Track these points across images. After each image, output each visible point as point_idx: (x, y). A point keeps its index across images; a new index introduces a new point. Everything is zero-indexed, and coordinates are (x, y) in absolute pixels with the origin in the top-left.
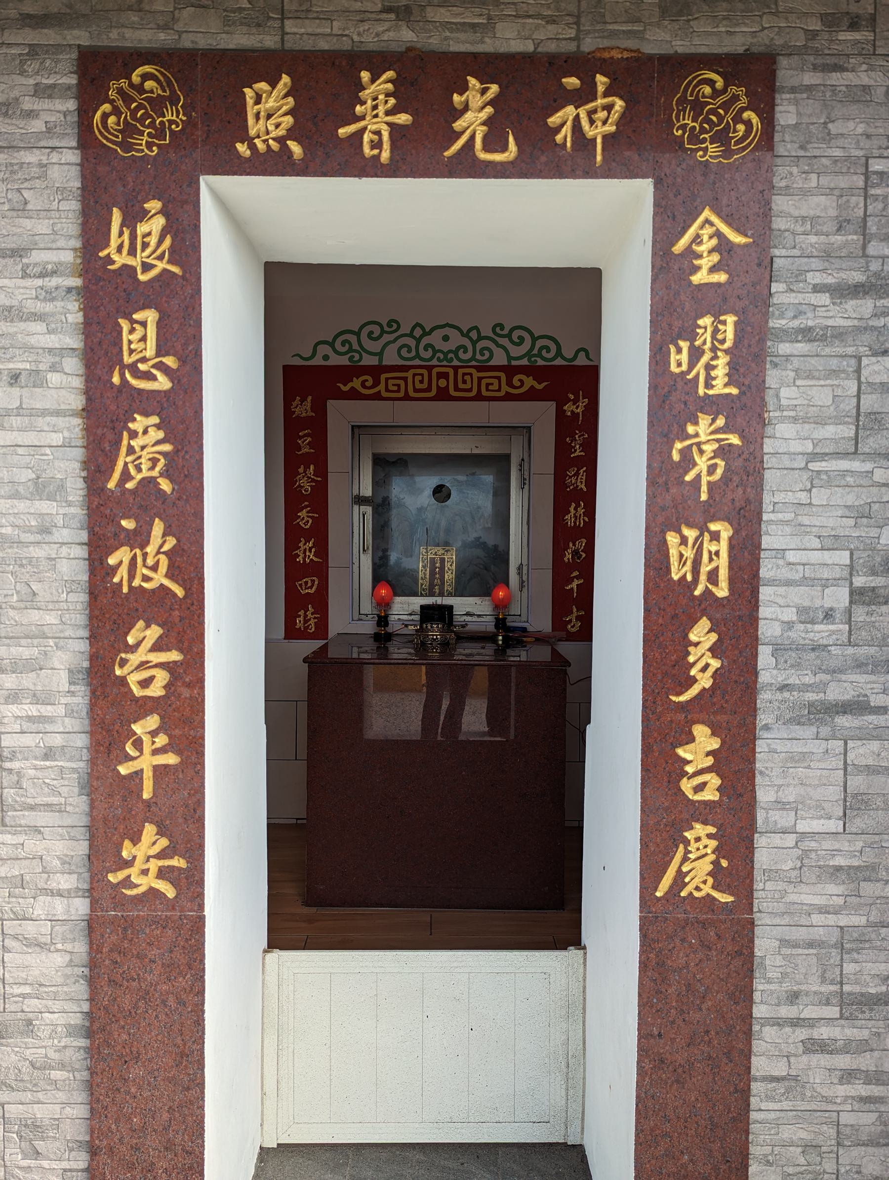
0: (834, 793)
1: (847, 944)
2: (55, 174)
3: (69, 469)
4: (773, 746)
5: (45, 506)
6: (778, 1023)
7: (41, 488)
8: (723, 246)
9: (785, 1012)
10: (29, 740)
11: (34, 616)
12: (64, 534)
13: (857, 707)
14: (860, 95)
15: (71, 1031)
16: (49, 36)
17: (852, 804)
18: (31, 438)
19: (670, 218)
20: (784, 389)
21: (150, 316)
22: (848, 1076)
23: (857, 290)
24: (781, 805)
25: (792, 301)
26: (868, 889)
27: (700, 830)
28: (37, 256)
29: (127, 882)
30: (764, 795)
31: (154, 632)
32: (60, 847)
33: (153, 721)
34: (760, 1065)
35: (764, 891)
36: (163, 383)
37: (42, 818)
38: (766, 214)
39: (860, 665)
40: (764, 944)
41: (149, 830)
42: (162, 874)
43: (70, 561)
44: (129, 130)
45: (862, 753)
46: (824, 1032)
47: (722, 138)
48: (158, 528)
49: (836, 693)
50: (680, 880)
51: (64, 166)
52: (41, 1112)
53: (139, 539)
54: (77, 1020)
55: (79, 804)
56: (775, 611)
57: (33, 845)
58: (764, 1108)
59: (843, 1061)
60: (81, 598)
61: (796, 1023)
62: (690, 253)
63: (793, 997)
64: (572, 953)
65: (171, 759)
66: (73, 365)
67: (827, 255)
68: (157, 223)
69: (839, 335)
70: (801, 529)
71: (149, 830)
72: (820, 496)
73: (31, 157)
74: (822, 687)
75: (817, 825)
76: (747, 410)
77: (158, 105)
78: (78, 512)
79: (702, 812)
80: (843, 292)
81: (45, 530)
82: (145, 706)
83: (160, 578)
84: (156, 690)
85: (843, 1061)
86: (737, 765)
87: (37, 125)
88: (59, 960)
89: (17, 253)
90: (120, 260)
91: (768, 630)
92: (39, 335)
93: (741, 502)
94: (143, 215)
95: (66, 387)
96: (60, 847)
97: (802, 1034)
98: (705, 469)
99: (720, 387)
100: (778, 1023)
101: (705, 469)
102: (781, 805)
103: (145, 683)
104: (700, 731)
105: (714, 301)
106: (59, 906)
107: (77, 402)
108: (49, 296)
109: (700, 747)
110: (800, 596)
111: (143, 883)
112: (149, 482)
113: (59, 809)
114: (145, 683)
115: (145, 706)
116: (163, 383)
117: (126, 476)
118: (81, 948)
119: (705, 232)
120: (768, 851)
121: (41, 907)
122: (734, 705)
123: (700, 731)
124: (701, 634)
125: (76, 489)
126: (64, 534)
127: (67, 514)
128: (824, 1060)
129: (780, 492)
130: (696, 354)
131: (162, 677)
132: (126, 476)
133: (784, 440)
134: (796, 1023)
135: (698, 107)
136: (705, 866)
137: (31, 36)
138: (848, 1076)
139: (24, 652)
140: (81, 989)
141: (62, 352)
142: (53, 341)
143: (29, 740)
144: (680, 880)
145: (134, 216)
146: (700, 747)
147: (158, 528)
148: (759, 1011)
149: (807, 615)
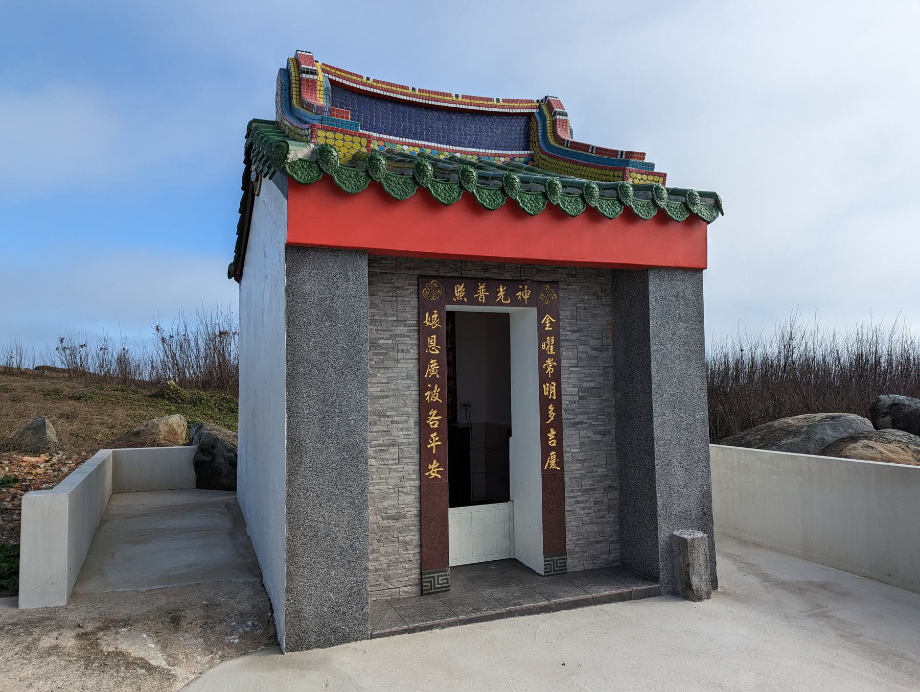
0: (578, 443)
1: (582, 477)
2: (412, 303)
3: (414, 373)
4: (566, 432)
5: (409, 382)
6: (569, 497)
7: (408, 377)
8: (551, 322)
9: (571, 494)
10: (405, 441)
11: (406, 409)
12: (413, 388)
13: (581, 423)
14: (574, 291)
15: (415, 516)
16: (411, 272)
17: (582, 445)
18: (406, 365)
19: (540, 316)
20: (564, 353)
21: (434, 336)
22: (584, 508)
23: (576, 331)
24: (568, 446)
25: (565, 333)
26: (585, 464)
27: (553, 453)
28: (408, 322)
29: (430, 475)
30: (565, 444)
31: (435, 412)
32: (412, 468)
33: (435, 434)
34: (567, 508)
35: (566, 466)
36: (437, 352)
37: (408, 461)
38: (559, 315)
39: (581, 413)
40: (566, 479)
41: (435, 461)
42: (438, 472)
43: (413, 393)
44: (430, 294)
45: (583, 433)
46: (579, 499)
47: (549, 299)
48: (436, 387)
49: (577, 420)
50: (549, 465)
51: (414, 302)
52: (408, 538)
53: (432, 389)
54: (416, 513)
55: (417, 456)
56: (565, 401)
57: (406, 468)
58: (568, 518)
59: (583, 505)
60: (416, 404)
61: (573, 497)
62: (545, 323)
63: (572, 491)
64: (190, 475)
65: (439, 443)
66: (415, 347)
67: (570, 324)
68: (435, 316)
69: (573, 340)
70: (568, 383)
71: (435, 461)
72: (572, 376)
73: (407, 299)
74: (574, 419)
75: (575, 450)
76: (557, 358)
77: (436, 289)
78: (416, 383)
79: (553, 449)
80: (573, 332)
81: (409, 387)
82: (434, 430)
83: (437, 398)
84: (436, 426)
85: (583, 505)
86: (559, 437)
87: (408, 292)
88: (412, 497)
89: (403, 321)
90: (428, 324)
91: (564, 406)
92: (408, 341)
93: (557, 377)
94: (433, 314)
95: (413, 353)
96: (412, 468)
97: (390, 419)
98: (550, 370)
99: (552, 353)
100: (569, 497)
101: (550, 370)
102: (568, 446)
103: (433, 424)
104: (552, 430)
105: (549, 333)
106: (412, 482)
107: (416, 356)
108: (410, 331)
109: (552, 433)
110: (569, 398)
111: (433, 475)
112: (434, 375)
113: (412, 458)
114: (433, 424)
115: (434, 430)
116: (437, 352)
117: (429, 374)
118: (418, 493)
119: (547, 319)
120: (567, 457)
121: (408, 484)
122: (558, 424)
123: (552, 430)
124: (551, 407)
125: (416, 377)
126: (413, 388)
127: (413, 383)
128: (579, 505)
129: (565, 375)
130: (547, 345)
131: (437, 423)
132: (429, 374)
133: (565, 363)
134: (573, 497)
135: (544, 292)
136: (554, 461)
137: (408, 272)
138: (584, 508)
139: (404, 418)
140: (418, 505)
141: (413, 345)
142: (411, 342)
143: (405, 441)
144: (549, 465)
145: (431, 314)
146: (552, 433)
147: (436, 387)
148: (566, 495)
149: (571, 402)
